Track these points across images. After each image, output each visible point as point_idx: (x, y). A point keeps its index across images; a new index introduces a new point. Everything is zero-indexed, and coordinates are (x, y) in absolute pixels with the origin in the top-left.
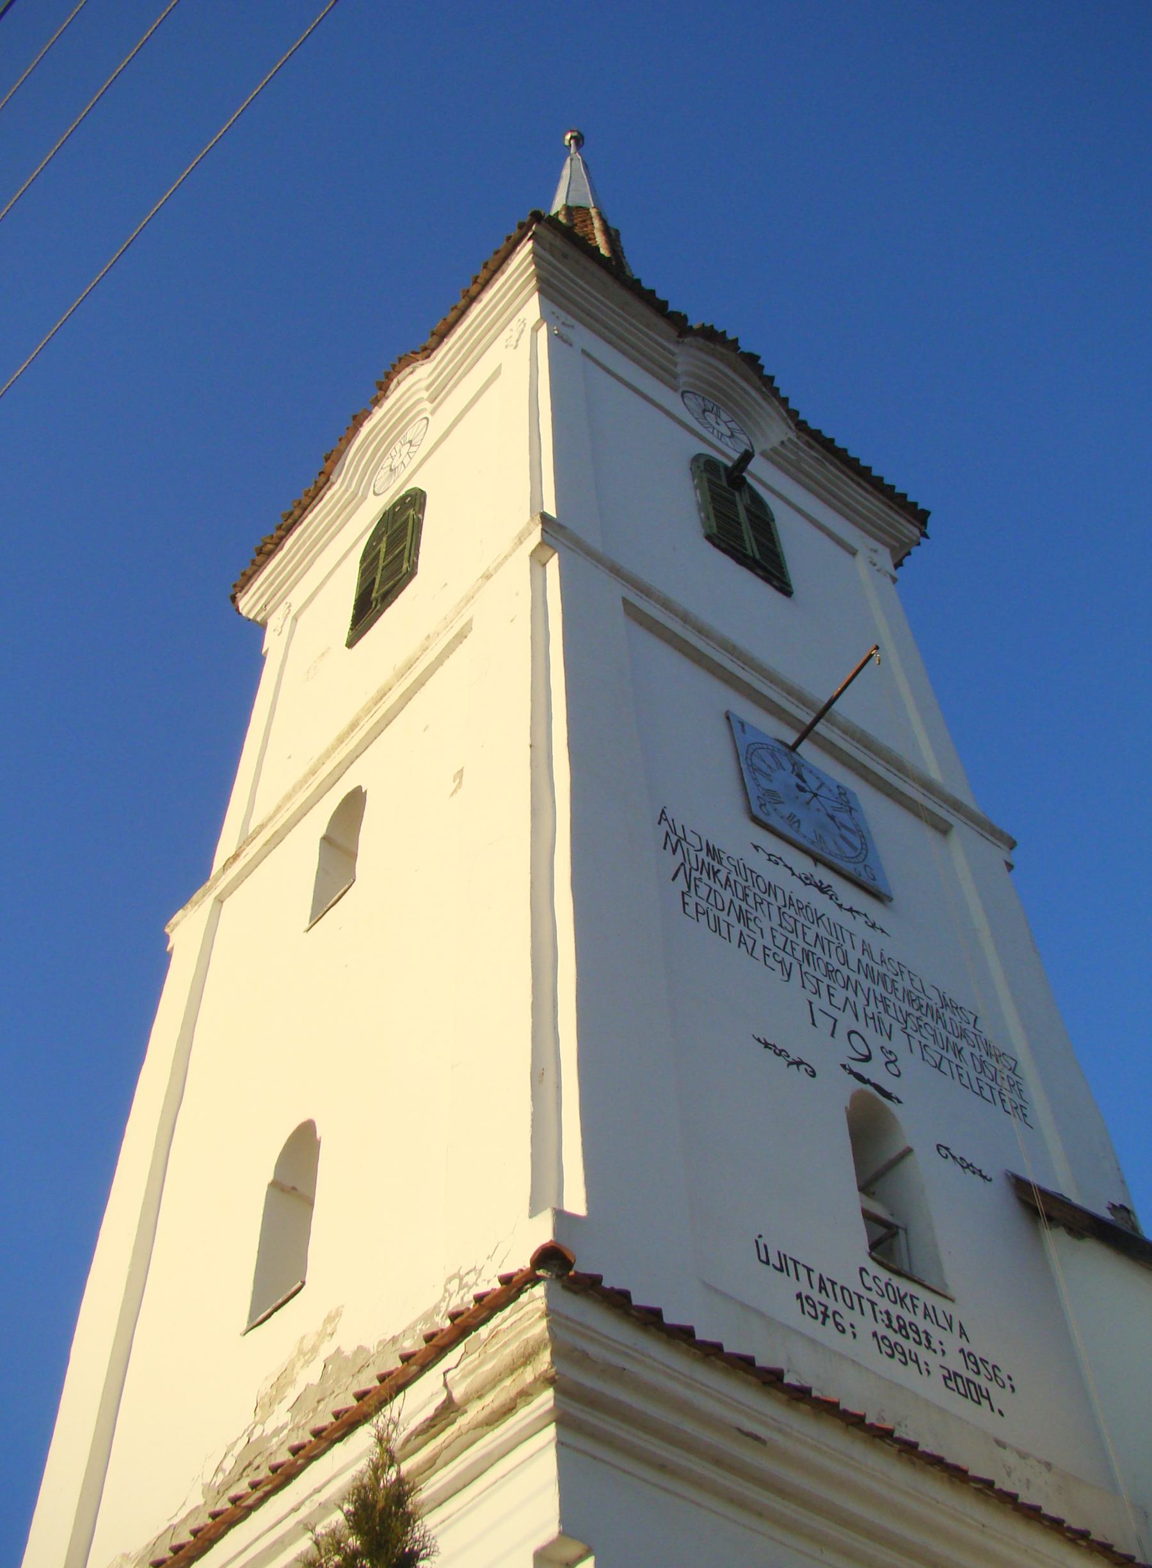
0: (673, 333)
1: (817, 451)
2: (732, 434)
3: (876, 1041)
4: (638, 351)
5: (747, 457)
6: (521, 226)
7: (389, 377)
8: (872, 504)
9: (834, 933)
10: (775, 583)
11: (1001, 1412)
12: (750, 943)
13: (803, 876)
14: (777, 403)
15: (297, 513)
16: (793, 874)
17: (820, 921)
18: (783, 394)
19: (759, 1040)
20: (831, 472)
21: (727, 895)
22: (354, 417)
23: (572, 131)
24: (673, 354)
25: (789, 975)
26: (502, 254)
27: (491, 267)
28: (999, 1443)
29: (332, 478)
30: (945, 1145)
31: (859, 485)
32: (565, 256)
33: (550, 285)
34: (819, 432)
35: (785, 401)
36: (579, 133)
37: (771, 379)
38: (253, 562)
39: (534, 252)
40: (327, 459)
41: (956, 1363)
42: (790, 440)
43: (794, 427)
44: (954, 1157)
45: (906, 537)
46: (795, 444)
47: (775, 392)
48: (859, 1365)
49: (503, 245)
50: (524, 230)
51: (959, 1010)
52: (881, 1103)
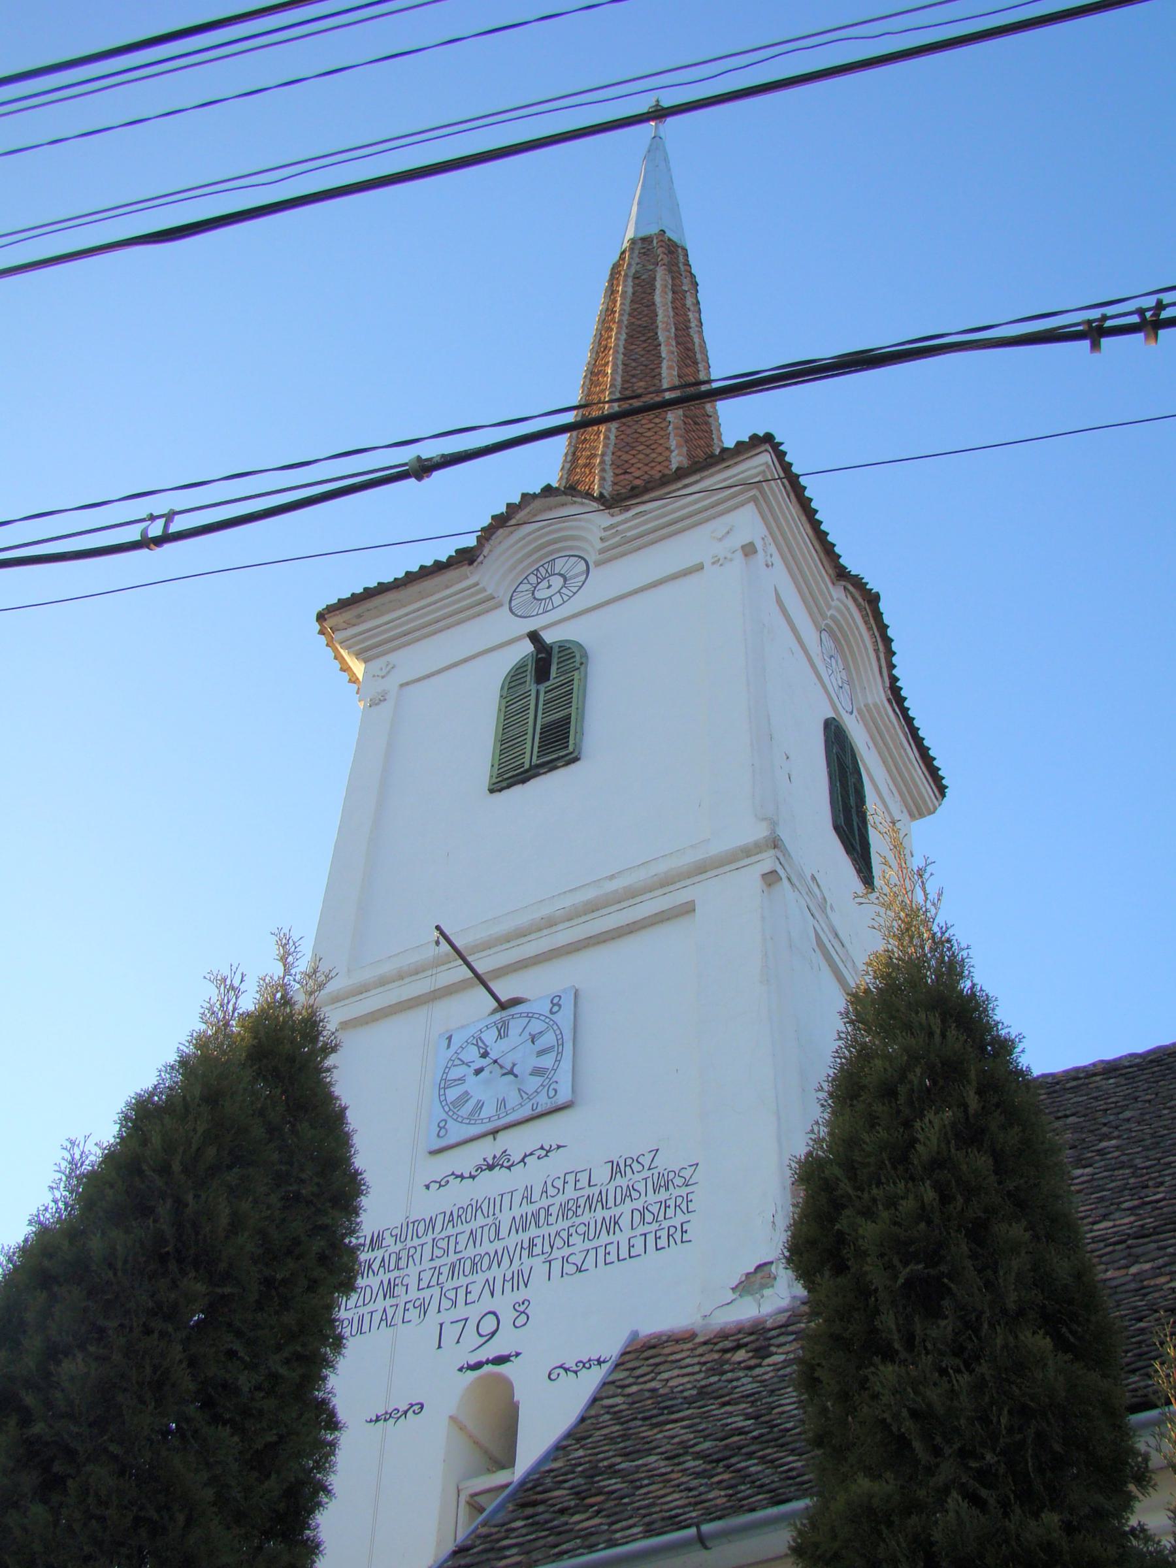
0: (466, 569)
5: (534, 637)
12: (390, 1312)
19: (371, 1421)
24: (477, 584)
32: (359, 616)
42: (605, 529)
44: (566, 1370)
46: (612, 527)
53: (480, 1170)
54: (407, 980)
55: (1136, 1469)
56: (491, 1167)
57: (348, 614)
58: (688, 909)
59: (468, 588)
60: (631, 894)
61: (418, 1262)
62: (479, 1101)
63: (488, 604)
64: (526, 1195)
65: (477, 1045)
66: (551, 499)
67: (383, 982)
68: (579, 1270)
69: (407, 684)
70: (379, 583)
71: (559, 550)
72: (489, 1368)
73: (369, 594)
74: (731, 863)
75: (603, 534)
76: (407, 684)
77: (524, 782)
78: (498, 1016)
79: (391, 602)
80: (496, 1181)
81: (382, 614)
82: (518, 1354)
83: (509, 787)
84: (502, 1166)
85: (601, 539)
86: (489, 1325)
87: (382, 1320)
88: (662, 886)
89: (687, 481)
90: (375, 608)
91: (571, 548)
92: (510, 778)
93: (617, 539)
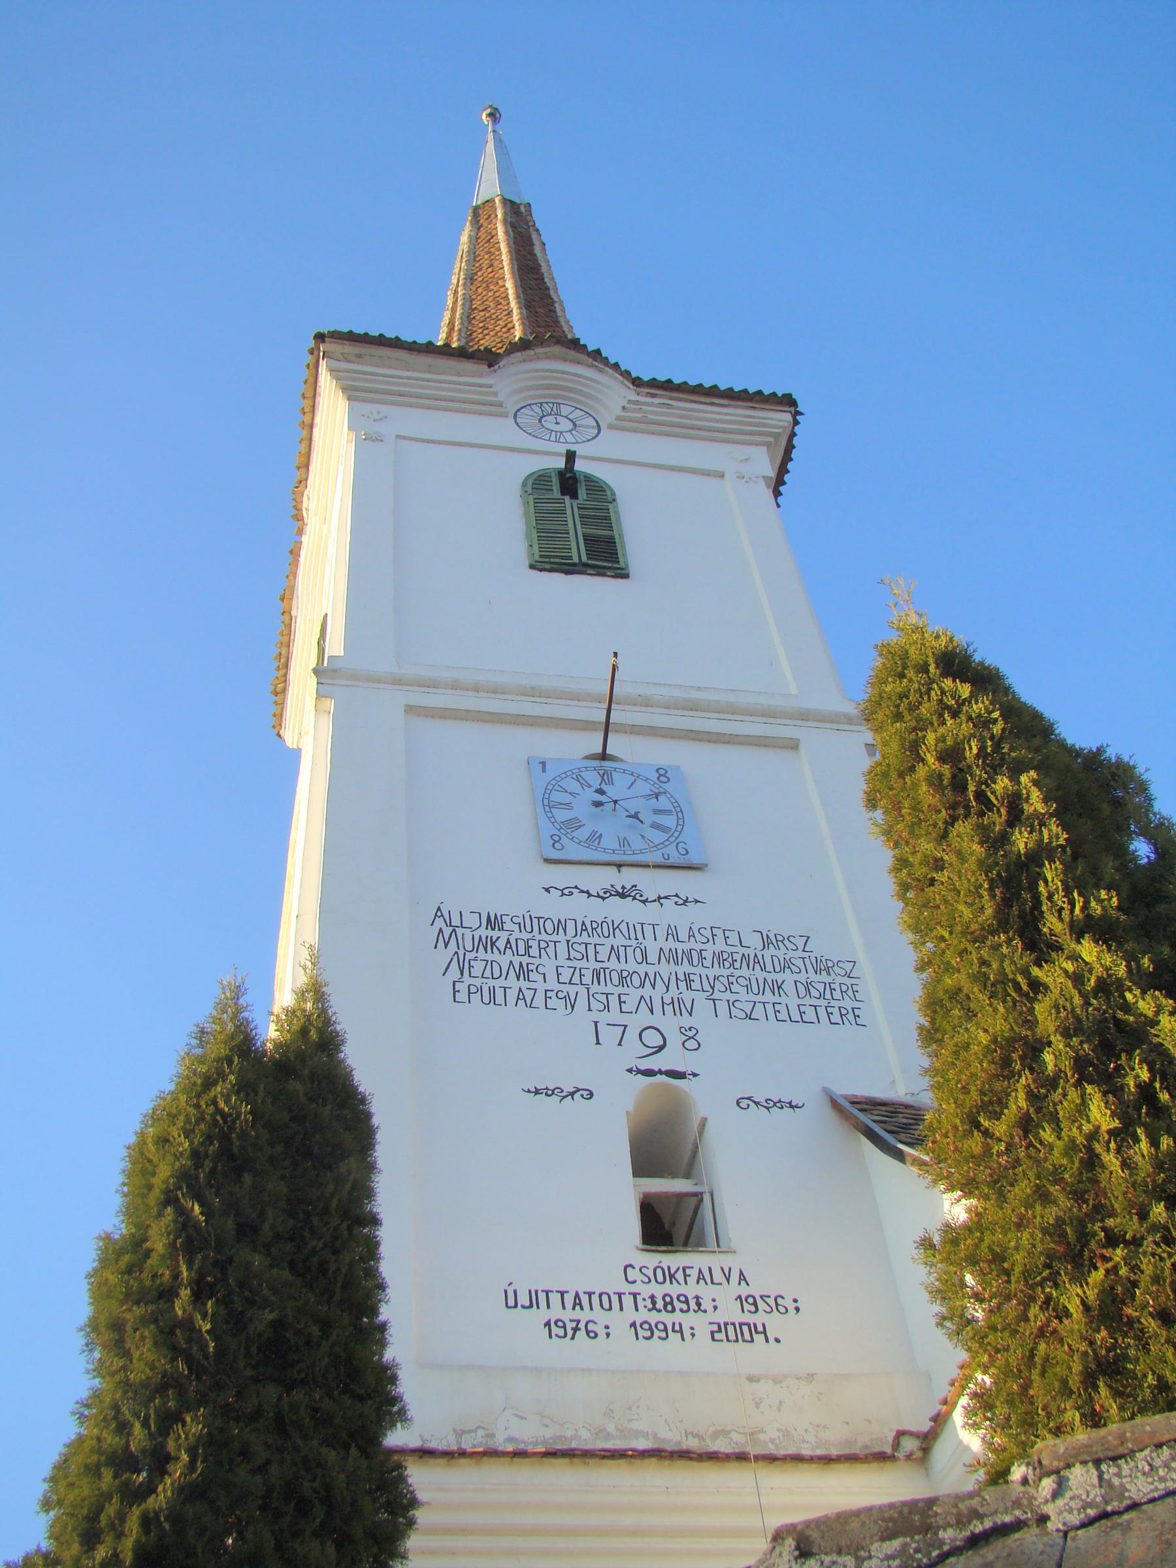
0: (484, 368)
1: (662, 397)
2: (575, 425)
3: (670, 1024)
4: (459, 402)
5: (571, 457)
6: (311, 352)
7: (298, 508)
8: (737, 414)
9: (633, 936)
10: (609, 574)
11: (777, 1340)
12: (528, 995)
13: (601, 894)
14: (611, 371)
15: (284, 651)
16: (590, 895)
17: (617, 931)
18: (612, 361)
19: (529, 1091)
20: (683, 406)
21: (504, 960)
22: (291, 552)
23: (484, 110)
24: (490, 386)
25: (573, 1007)
26: (311, 381)
27: (309, 394)
28: (752, 1379)
29: (294, 613)
30: (746, 1096)
31: (712, 404)
32: (359, 356)
33: (355, 389)
34: (654, 379)
35: (616, 366)
36: (491, 107)
37: (598, 352)
38: (276, 703)
39: (331, 370)
40: (282, 600)
41: (731, 1312)
42: (629, 402)
43: (631, 386)
44: (757, 1103)
45: (778, 427)
46: (636, 403)
47: (605, 361)
48: (589, 1370)
49: (306, 373)
50: (316, 353)
51: (786, 942)
52: (675, 1087)
53: (608, 894)
54: (482, 694)
55: (890, 1524)
56: (623, 896)
57: (349, 349)
58: (792, 745)
59: (480, 386)
60: (734, 711)
61: (552, 955)
62: (594, 833)
63: (494, 408)
64: (670, 932)
65: (578, 780)
66: (573, 352)
67: (455, 686)
68: (749, 1017)
69: (404, 438)
70: (397, 337)
71: (569, 399)
72: (663, 1078)
73: (381, 341)
74: (832, 722)
75: (627, 405)
76: (404, 438)
77: (567, 573)
78: (596, 763)
79: (398, 359)
80: (617, 909)
81: (383, 366)
82: (695, 1075)
83: (550, 571)
84: (634, 898)
85: (624, 408)
86: (653, 1039)
87: (518, 998)
88: (764, 715)
89: (715, 400)
90: (380, 357)
91: (578, 402)
92: (553, 563)
93: (639, 415)
